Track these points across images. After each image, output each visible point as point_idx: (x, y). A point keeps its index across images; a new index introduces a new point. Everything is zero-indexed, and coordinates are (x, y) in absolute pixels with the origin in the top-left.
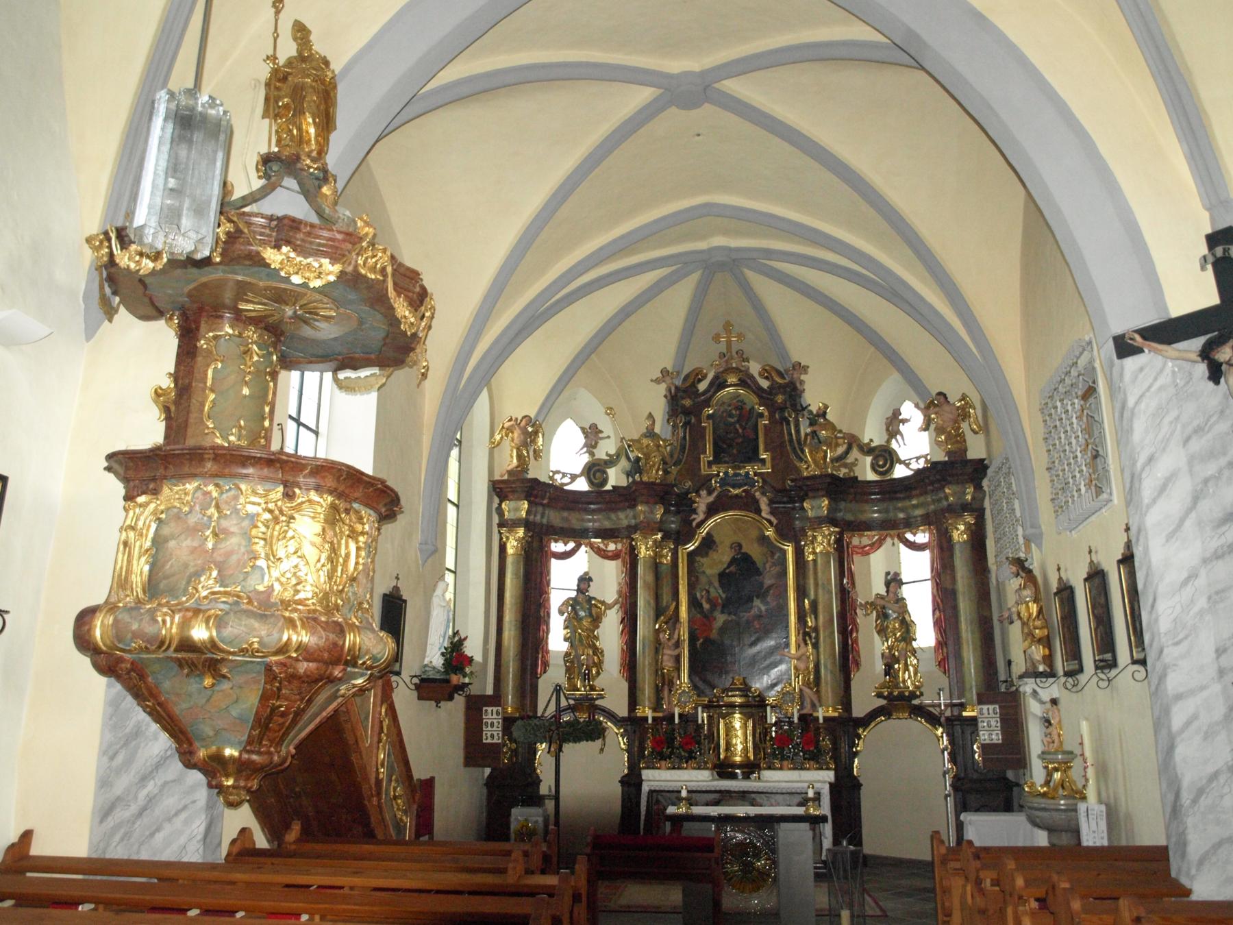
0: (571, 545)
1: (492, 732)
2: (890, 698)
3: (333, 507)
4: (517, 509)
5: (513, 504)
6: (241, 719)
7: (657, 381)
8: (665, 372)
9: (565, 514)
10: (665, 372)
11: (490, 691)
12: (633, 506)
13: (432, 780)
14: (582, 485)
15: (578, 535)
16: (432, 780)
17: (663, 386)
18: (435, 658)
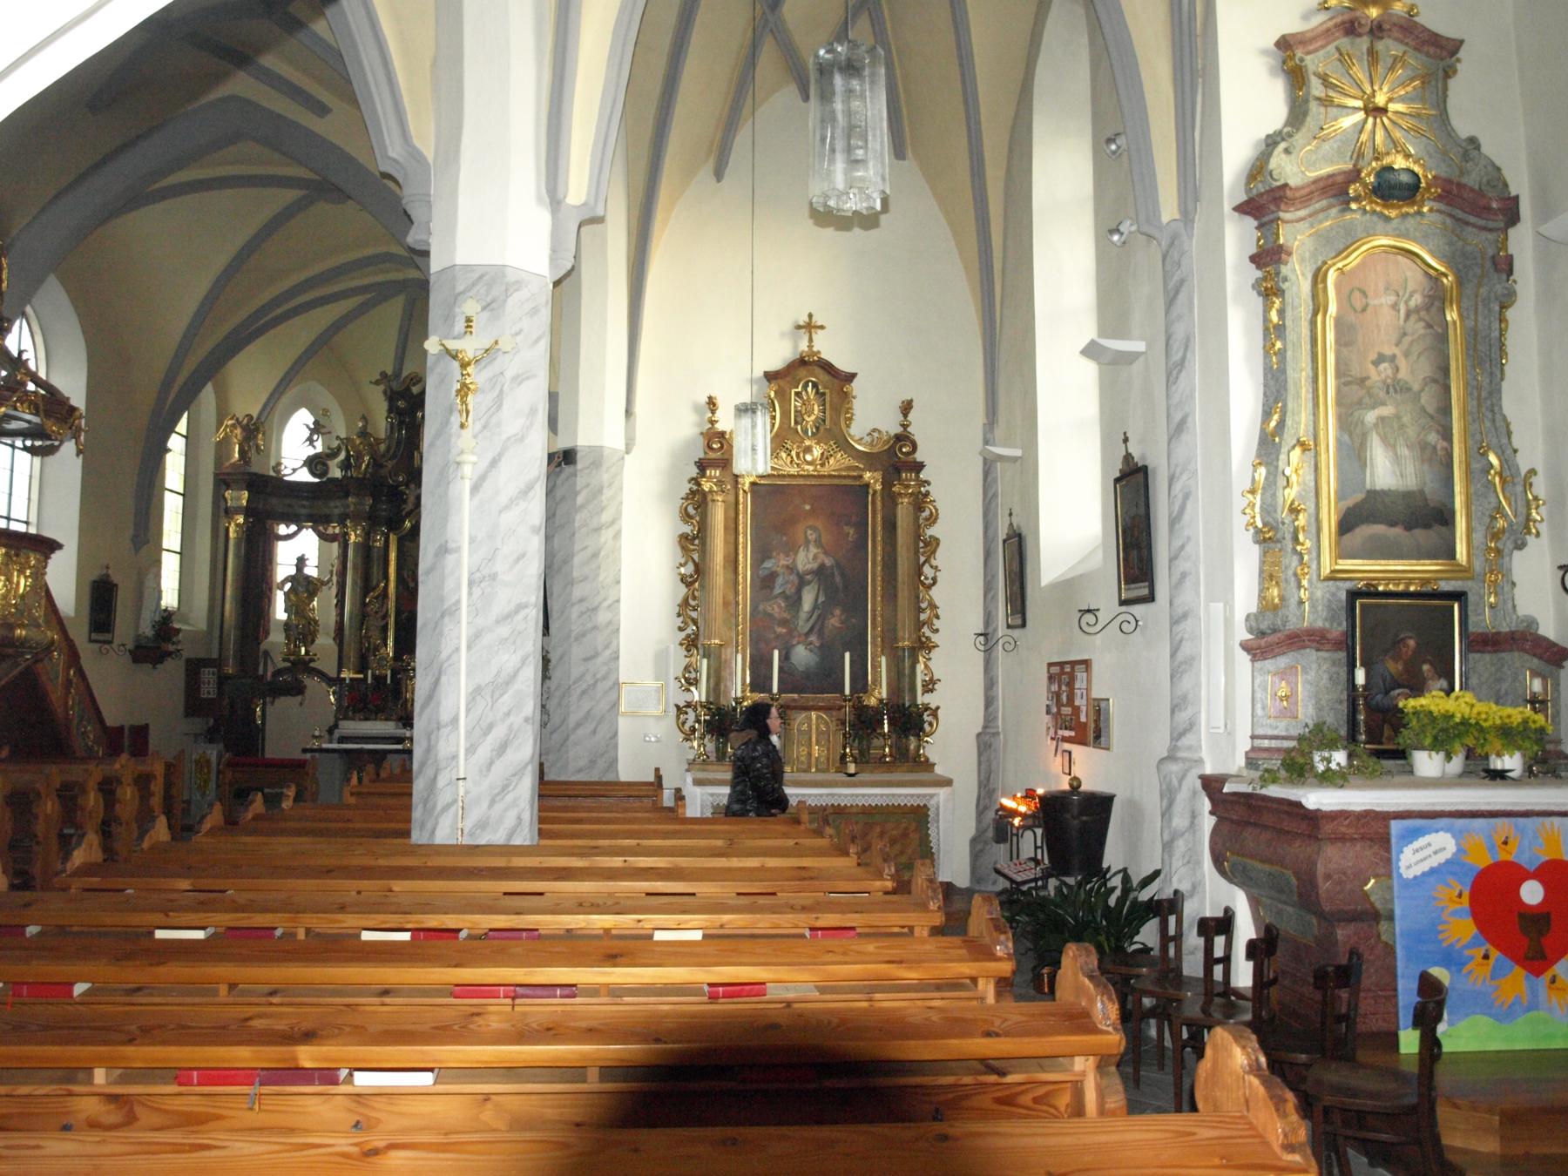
0: (293, 528)
1: (209, 690)
2: (293, 663)
3: (7, 554)
4: (239, 498)
5: (235, 494)
6: (526, 720)
7: (377, 383)
8: (384, 375)
9: (288, 501)
10: (384, 375)
11: (215, 655)
12: (347, 495)
13: (147, 726)
14: (304, 476)
15: (298, 520)
16: (147, 726)
17: (382, 387)
18: (147, 630)
